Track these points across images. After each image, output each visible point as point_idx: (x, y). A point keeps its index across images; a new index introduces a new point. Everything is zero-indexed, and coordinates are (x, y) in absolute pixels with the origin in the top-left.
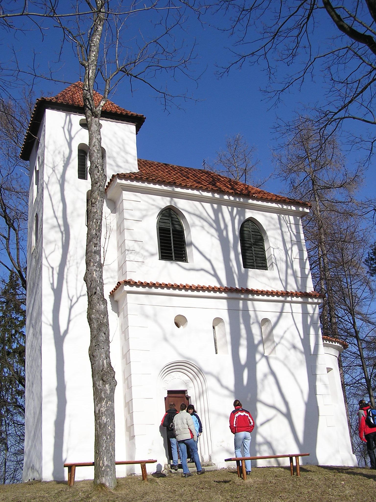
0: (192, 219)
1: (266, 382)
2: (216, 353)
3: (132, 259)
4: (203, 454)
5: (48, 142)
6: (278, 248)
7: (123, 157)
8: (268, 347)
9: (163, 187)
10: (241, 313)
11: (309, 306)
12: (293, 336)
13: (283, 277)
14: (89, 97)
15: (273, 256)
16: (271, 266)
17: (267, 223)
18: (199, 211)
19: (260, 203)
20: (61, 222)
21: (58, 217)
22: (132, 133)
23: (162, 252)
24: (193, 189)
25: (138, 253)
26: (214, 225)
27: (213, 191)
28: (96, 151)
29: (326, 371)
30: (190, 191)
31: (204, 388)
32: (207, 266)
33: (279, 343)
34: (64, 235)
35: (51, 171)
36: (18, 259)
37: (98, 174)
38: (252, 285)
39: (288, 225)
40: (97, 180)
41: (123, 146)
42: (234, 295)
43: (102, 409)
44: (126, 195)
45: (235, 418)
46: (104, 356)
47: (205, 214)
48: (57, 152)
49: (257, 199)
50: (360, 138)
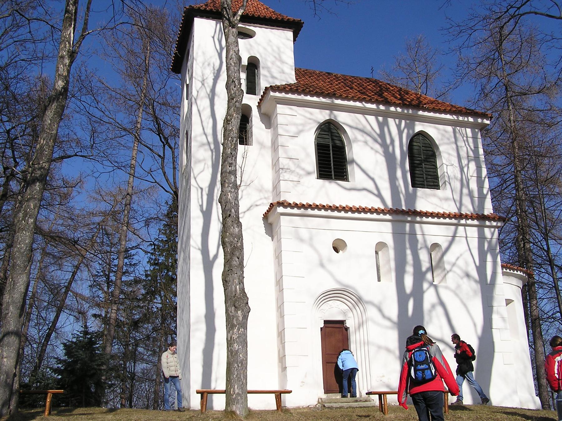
0: (354, 135)
1: (434, 313)
2: (379, 280)
3: (286, 178)
4: (361, 389)
5: (197, 53)
6: (452, 165)
7: (279, 67)
8: (438, 275)
9: (322, 99)
10: (407, 237)
11: (487, 230)
12: (467, 263)
13: (457, 197)
14: (226, 6)
15: (446, 174)
16: (444, 185)
17: (440, 137)
18: (362, 125)
19: (431, 114)
20: (211, 139)
21: (208, 134)
22: (288, 39)
23: (320, 171)
24: (355, 101)
25: (292, 172)
26: (379, 140)
27: (378, 102)
28: (233, 64)
29: (504, 303)
30: (351, 103)
31: (364, 318)
32: (370, 185)
33: (450, 270)
34: (214, 153)
35: (200, 84)
36: (174, 179)
37: (235, 89)
38: (421, 205)
39: (465, 138)
40: (234, 95)
41: (279, 55)
42: (400, 217)
43: (234, 336)
44: (281, 109)
45: (557, 364)
46: (236, 281)
47: (369, 128)
48: (206, 64)
49: (429, 110)
50: (551, 36)
